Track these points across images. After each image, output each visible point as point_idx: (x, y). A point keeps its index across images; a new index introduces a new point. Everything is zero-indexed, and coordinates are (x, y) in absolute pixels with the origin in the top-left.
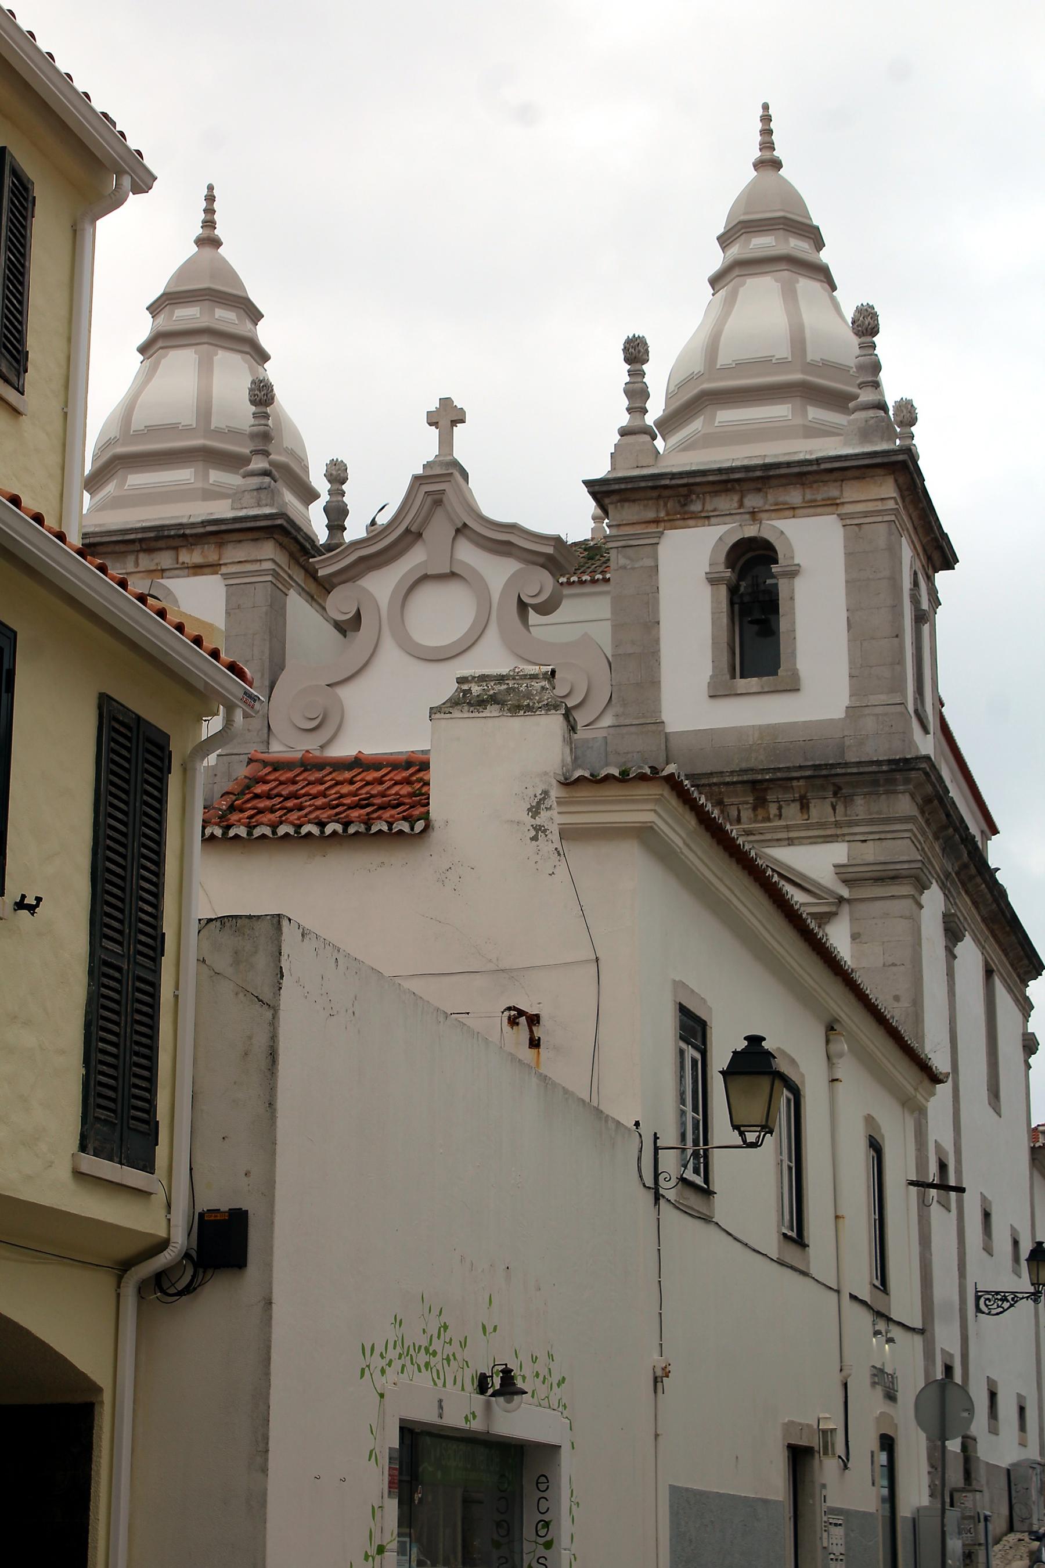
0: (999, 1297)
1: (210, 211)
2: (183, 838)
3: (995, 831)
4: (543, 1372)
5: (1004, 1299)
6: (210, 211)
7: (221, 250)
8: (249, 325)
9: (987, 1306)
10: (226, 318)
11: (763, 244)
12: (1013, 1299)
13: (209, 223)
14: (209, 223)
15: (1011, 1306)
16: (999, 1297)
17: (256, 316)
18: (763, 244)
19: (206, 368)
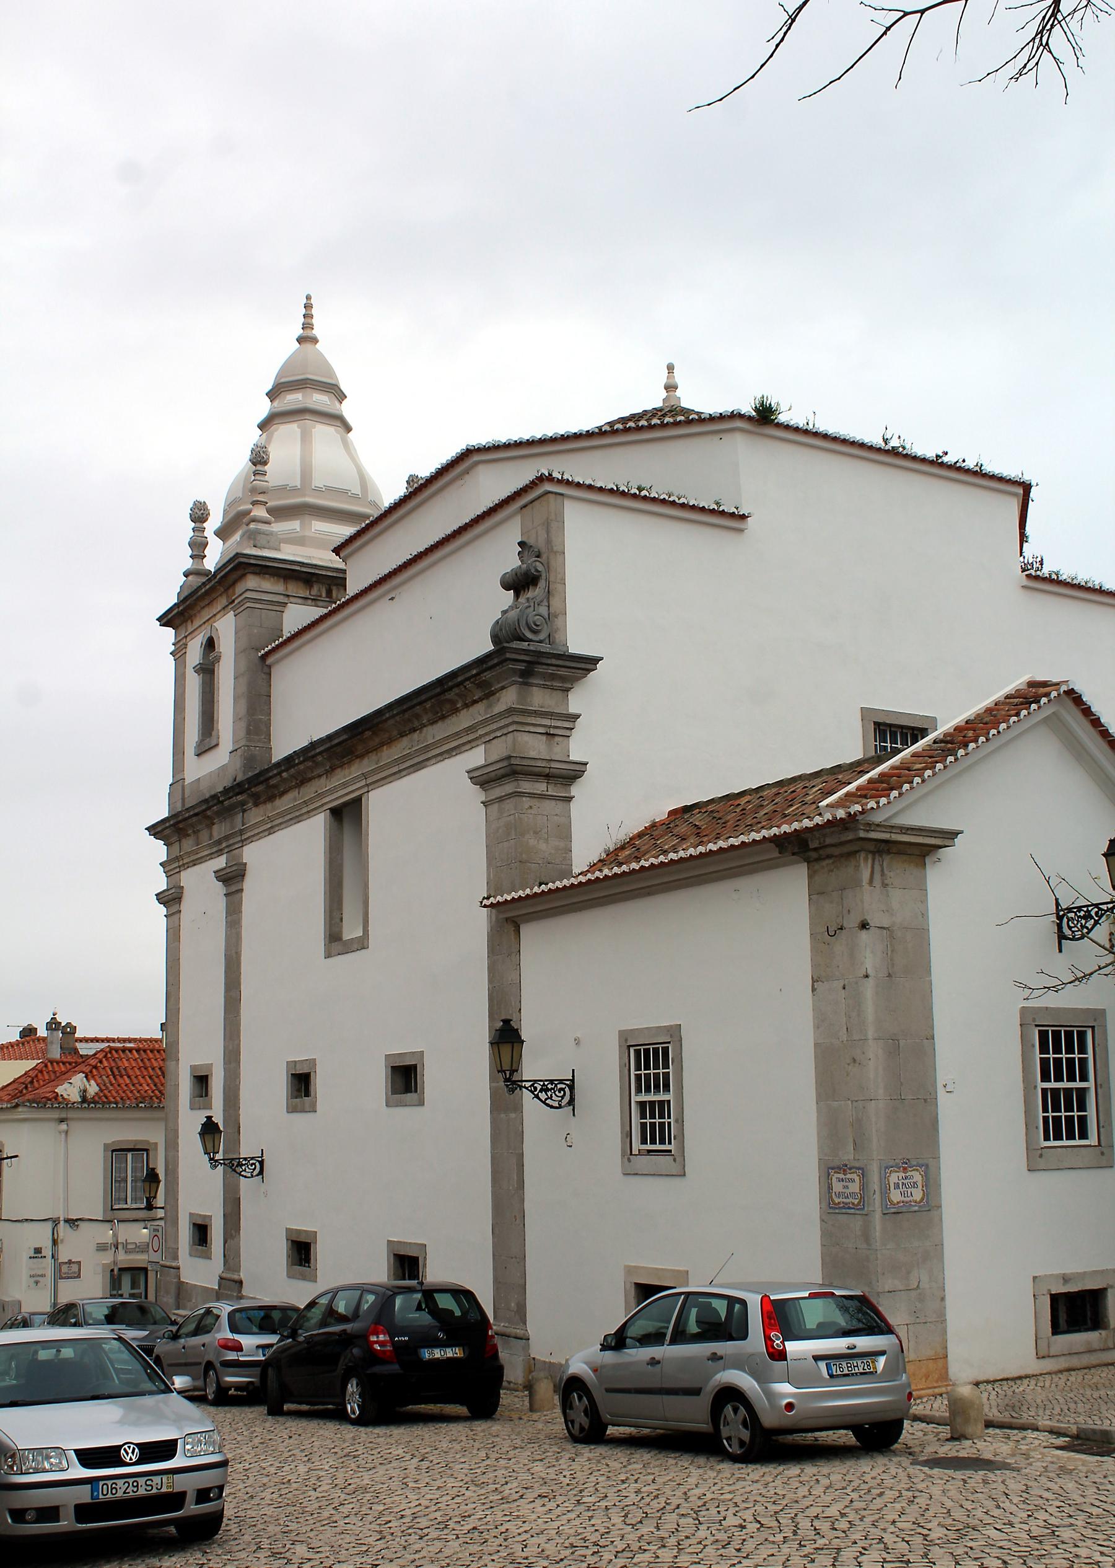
0: (1082, 914)
1: (308, 316)
2: (600, 433)
3: (1023, 491)
4: (500, 1540)
5: (1088, 916)
6: (308, 316)
7: (318, 346)
8: (337, 403)
9: (1070, 928)
10: (320, 400)
11: (294, 399)
12: (1096, 913)
13: (307, 326)
14: (307, 326)
15: (1096, 923)
16: (1082, 914)
17: (341, 396)
18: (294, 399)
19: (306, 438)
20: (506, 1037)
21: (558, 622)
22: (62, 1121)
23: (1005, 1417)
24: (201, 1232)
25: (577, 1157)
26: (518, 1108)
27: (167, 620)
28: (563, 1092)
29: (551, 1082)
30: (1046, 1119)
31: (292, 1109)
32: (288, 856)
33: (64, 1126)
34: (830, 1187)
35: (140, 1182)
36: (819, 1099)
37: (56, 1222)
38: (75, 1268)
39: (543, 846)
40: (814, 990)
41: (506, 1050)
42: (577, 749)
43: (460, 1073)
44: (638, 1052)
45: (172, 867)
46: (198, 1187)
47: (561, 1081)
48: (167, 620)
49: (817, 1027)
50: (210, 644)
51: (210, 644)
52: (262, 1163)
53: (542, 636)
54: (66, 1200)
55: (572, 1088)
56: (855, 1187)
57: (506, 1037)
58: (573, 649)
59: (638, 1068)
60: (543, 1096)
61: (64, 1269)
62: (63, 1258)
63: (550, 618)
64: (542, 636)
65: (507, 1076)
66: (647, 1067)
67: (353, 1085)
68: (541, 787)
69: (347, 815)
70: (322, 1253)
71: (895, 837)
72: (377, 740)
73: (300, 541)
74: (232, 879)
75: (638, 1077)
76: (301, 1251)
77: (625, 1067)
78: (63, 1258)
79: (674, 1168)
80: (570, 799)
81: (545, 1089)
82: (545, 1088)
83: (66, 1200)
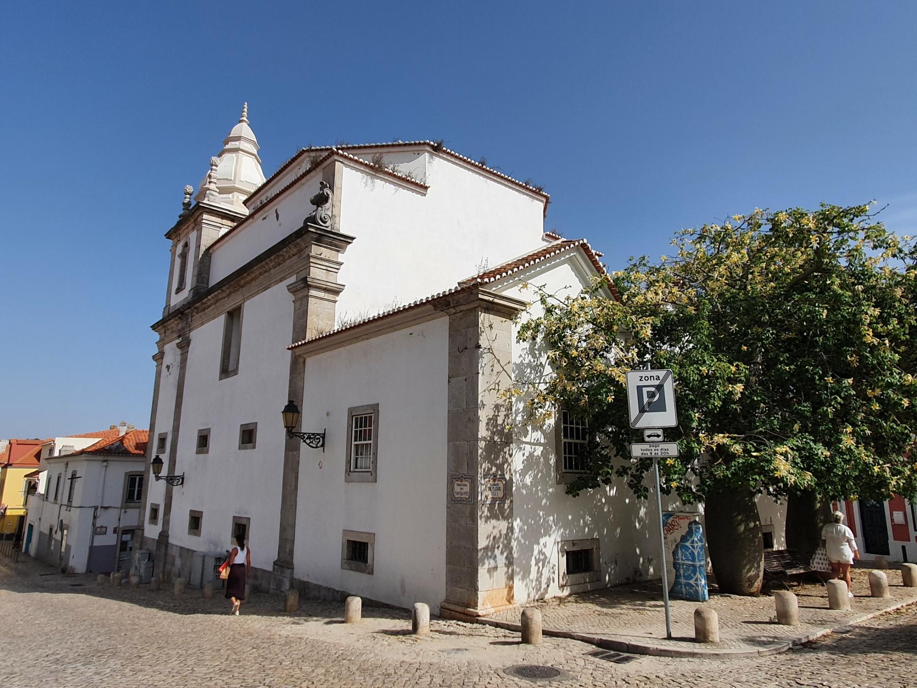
20: (292, 409)
21: (337, 219)
22: (105, 461)
23: (671, 619)
24: (155, 511)
25: (322, 469)
26: (298, 449)
27: (169, 236)
28: (319, 439)
29: (313, 434)
30: (565, 458)
31: (198, 452)
32: (208, 335)
33: (105, 464)
34: (453, 489)
35: (134, 489)
36: (448, 563)
37: (96, 508)
38: (104, 529)
39: (320, 322)
40: (449, 382)
41: (290, 415)
42: (341, 278)
43: (272, 434)
44: (357, 419)
45: (161, 343)
46: (155, 491)
47: (318, 434)
48: (169, 236)
49: (449, 402)
50: (186, 245)
51: (186, 245)
52: (183, 479)
53: (327, 225)
54: (103, 497)
55: (324, 438)
56: (467, 489)
57: (292, 409)
58: (342, 232)
59: (356, 427)
60: (308, 441)
61: (98, 530)
62: (98, 524)
63: (332, 217)
64: (327, 225)
65: (293, 433)
66: (361, 427)
67: (225, 440)
68: (321, 294)
69: (234, 315)
70: (205, 524)
71: (496, 301)
72: (249, 278)
73: (232, 203)
74: (184, 346)
75: (356, 432)
76: (195, 521)
77: (350, 426)
78: (98, 524)
79: (371, 478)
80: (335, 302)
81: (309, 438)
82: (312, 437)
83: (103, 497)
